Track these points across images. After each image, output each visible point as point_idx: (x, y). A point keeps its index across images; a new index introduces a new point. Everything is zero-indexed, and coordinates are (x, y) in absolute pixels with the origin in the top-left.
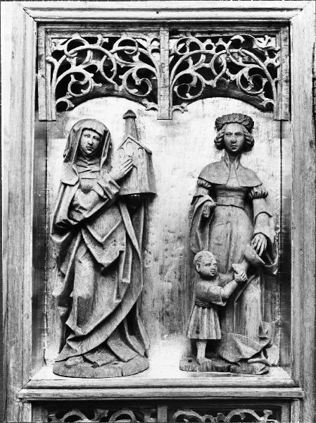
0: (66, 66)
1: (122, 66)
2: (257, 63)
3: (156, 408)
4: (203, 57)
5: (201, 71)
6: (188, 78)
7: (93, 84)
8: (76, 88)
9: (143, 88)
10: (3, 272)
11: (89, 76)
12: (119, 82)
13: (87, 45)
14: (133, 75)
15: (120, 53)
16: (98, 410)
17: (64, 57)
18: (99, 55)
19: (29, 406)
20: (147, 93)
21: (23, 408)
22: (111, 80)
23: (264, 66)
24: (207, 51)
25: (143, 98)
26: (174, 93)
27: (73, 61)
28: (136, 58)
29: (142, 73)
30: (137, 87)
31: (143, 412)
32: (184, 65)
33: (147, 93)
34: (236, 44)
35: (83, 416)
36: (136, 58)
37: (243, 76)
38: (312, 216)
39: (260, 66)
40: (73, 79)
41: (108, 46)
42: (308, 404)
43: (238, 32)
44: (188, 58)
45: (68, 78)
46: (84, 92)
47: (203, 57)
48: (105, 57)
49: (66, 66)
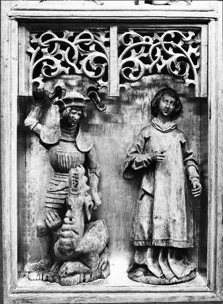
0: (40, 54)
1: (82, 55)
2: (182, 52)
3: (109, 30)
4: (143, 49)
5: (142, 59)
6: (131, 64)
7: (61, 68)
8: (49, 71)
9: (98, 72)
10: (6, 232)
11: (57, 62)
12: (79, 66)
13: (56, 38)
14: (90, 62)
15: (81, 44)
16: (66, 31)
17: (39, 48)
18: (64, 46)
19: (15, 24)
20: (101, 74)
21: (11, 24)
22: (73, 65)
23: (188, 54)
24: (146, 43)
25: (98, 79)
26: (121, 71)
27: (45, 50)
28: (92, 48)
29: (99, 60)
30: (93, 71)
31: (99, 33)
32: (128, 54)
33: (101, 74)
34: (168, 38)
35: (55, 36)
36: (92, 48)
37: (172, 62)
38: (221, 64)
39: (186, 55)
40: (45, 64)
41: (72, 39)
42: (220, 21)
43: (171, 29)
44: (131, 49)
45: (41, 64)
46: (53, 74)
47: (143, 49)
48: (68, 49)
49: (40, 54)
